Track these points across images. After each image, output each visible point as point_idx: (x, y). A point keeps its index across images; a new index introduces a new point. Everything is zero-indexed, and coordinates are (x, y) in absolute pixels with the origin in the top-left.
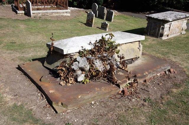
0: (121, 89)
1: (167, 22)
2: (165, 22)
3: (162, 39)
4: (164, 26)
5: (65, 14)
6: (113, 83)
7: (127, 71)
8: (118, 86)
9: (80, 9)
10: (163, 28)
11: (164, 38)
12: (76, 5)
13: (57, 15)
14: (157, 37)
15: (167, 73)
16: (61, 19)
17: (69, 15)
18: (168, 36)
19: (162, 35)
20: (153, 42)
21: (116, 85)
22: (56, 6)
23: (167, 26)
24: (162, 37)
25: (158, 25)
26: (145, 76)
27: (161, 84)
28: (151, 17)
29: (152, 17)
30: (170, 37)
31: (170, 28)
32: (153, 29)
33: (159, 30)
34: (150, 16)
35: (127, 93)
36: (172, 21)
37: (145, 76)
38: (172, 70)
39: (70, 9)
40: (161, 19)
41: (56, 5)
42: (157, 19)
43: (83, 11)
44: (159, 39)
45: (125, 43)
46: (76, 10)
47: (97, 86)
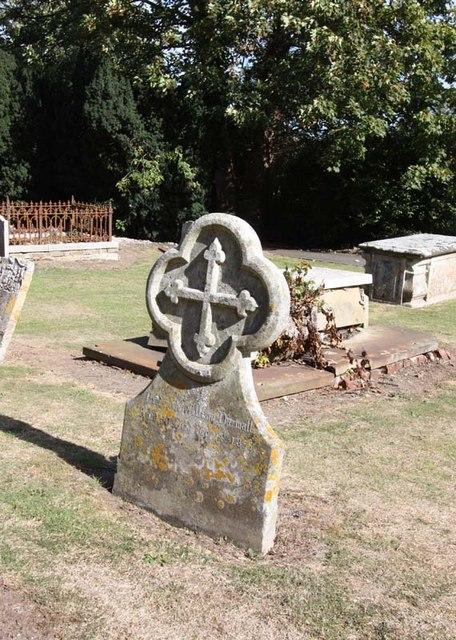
0: (338, 380)
1: (418, 258)
2: (413, 258)
3: (410, 306)
4: (412, 270)
5: (104, 256)
6: (320, 367)
7: (344, 349)
8: (331, 370)
9: (139, 242)
10: (410, 277)
11: (415, 303)
12: (123, 229)
13: (77, 257)
14: (396, 301)
15: (432, 357)
16: (89, 269)
17: (115, 257)
18: (425, 299)
19: (408, 296)
20: (387, 314)
21: (325, 369)
22: (64, 234)
23: (418, 269)
24: (410, 301)
25: (394, 269)
26: (384, 358)
27: (420, 376)
28: (373, 248)
29: (378, 248)
30: (431, 301)
31: (427, 275)
32: (389, 282)
33: (399, 282)
34: (371, 244)
35: (352, 384)
36: (430, 258)
37: (384, 358)
38: (442, 352)
39: (116, 241)
40: (403, 251)
41: (67, 230)
42: (389, 253)
43: (152, 248)
44: (401, 307)
45: (331, 289)
46: (131, 244)
47: (289, 372)
